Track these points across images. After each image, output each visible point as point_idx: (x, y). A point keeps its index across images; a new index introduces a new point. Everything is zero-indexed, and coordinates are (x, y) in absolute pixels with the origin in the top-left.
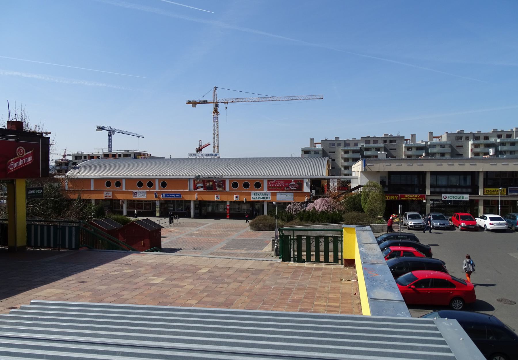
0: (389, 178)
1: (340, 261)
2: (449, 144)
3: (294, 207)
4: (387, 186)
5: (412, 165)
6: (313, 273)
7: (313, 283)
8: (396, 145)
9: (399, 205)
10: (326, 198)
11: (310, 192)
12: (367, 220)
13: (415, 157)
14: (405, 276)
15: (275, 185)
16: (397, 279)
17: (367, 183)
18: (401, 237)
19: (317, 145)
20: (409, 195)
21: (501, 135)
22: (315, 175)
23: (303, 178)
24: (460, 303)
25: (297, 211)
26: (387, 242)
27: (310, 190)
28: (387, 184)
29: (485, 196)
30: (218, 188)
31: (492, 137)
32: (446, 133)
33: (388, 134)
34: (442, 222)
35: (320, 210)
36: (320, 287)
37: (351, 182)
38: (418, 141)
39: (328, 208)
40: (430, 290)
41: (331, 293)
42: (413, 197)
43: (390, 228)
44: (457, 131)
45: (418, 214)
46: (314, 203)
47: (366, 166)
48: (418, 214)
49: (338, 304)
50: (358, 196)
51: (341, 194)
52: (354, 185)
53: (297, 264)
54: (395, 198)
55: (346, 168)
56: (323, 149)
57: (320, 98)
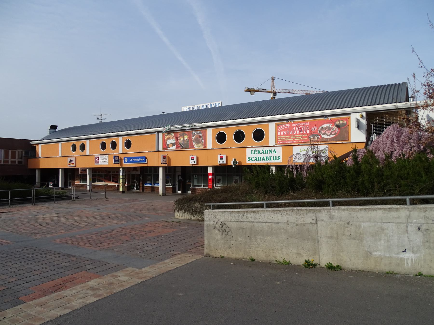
15: (291, 133)
23: (349, 114)
30: (196, 145)
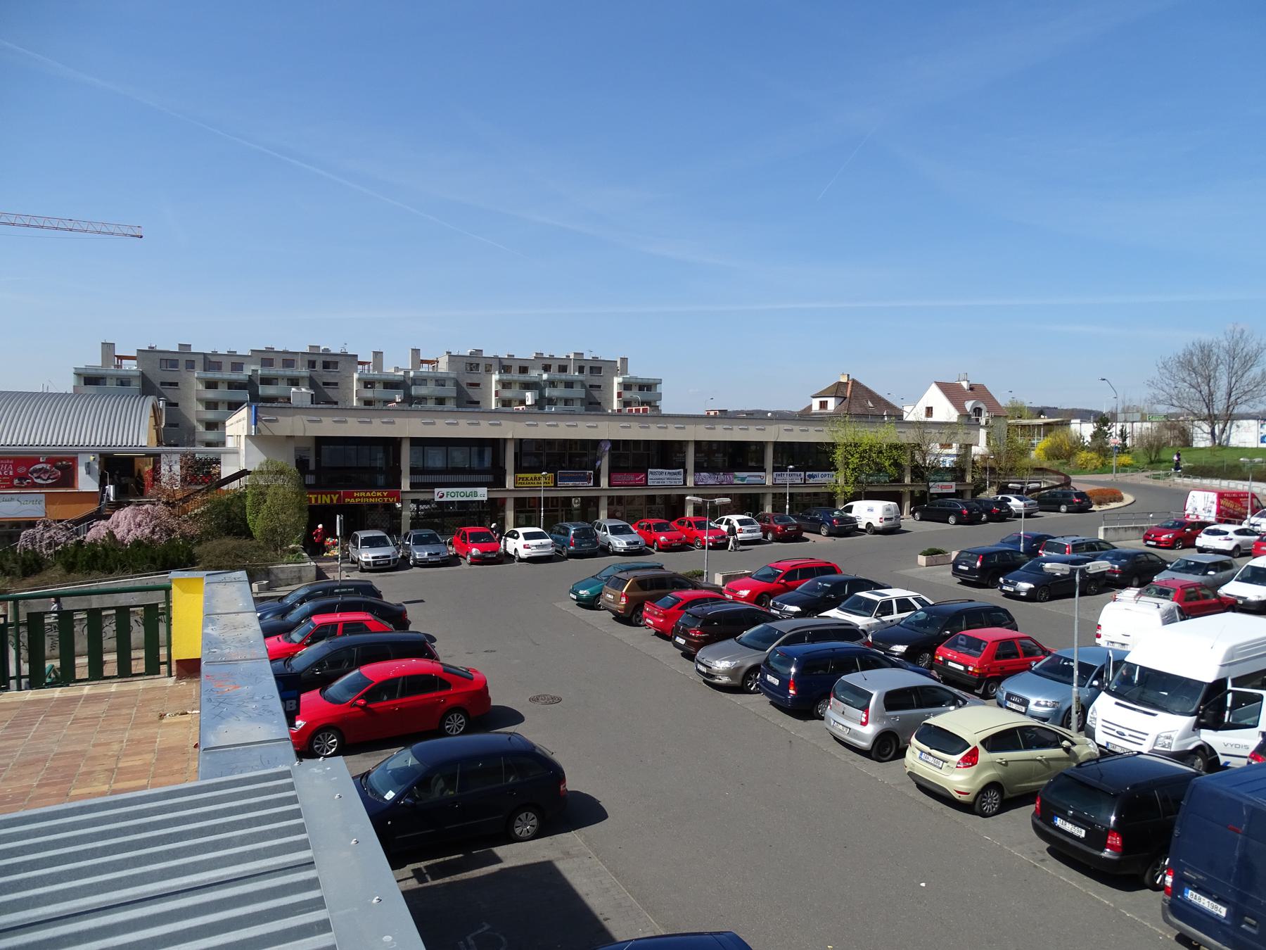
0: (318, 453)
1: (164, 668)
2: (454, 378)
3: (47, 535)
4: (311, 473)
5: (370, 422)
6: (80, 711)
7: (74, 738)
8: (339, 374)
9: (338, 517)
10: (147, 506)
11: (98, 490)
12: (262, 556)
13: (382, 403)
14: (351, 677)
16: (326, 689)
17: (261, 464)
18: (343, 590)
19: (123, 361)
20: (380, 492)
21: (550, 366)
22: (114, 444)
23: (77, 453)
24: (461, 719)
25: (57, 545)
26: (307, 606)
27: (100, 486)
28: (312, 466)
29: (698, 488)
31: (534, 368)
32: (447, 353)
33: (319, 347)
34: (433, 549)
35: (130, 538)
36: (94, 746)
37: (220, 463)
38: (389, 369)
39: (153, 532)
40: (398, 703)
41: (126, 755)
42: (372, 497)
43: (320, 574)
44: (469, 351)
45: (384, 534)
46: (110, 520)
47: (259, 423)
48: (384, 534)
49: (144, 782)
50: (239, 497)
51: (192, 494)
52: (226, 470)
53: (30, 695)
54: (332, 500)
55: (211, 426)
56: (142, 373)
57: (134, 234)
